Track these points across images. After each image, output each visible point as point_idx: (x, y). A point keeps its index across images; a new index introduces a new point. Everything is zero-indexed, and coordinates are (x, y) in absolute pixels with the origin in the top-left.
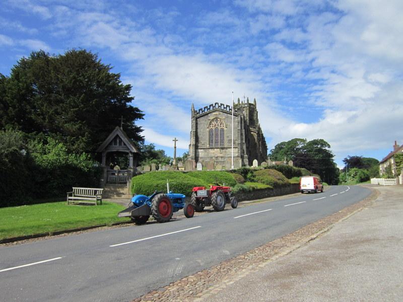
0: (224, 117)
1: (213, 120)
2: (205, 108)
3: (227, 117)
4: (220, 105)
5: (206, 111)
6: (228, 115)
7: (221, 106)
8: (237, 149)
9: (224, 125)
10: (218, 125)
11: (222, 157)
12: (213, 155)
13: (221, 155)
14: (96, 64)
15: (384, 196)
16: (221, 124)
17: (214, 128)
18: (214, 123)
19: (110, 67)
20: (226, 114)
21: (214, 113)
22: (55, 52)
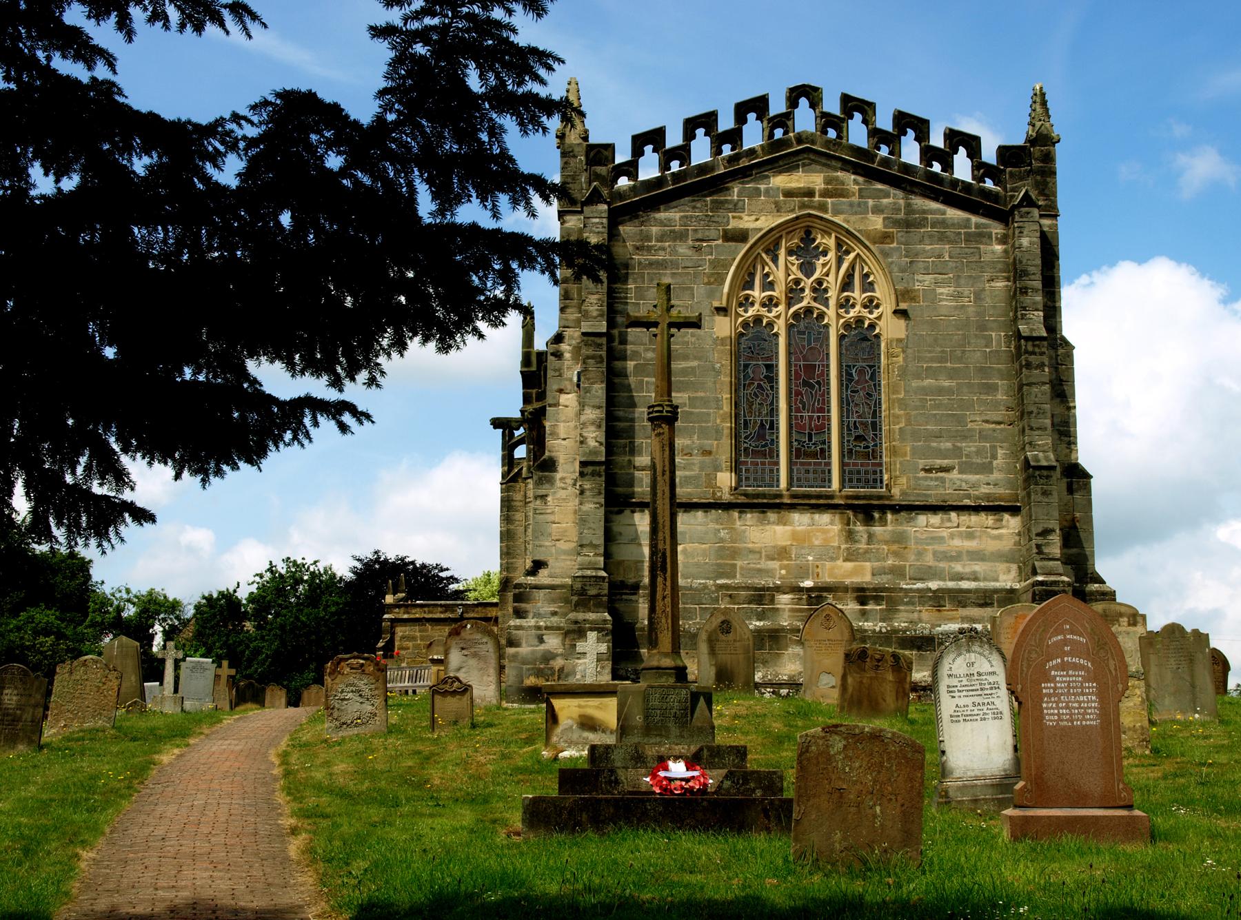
0: (877, 223)
1: (770, 243)
2: (742, 110)
3: (908, 225)
4: (937, 140)
5: (701, 151)
6: (919, 202)
7: (892, 140)
8: (1012, 523)
9: (883, 292)
10: (819, 290)
11: (863, 595)
12: (777, 573)
13: (862, 573)
14: (451, 206)
15: (542, 72)
16: (847, 285)
17: (780, 318)
18: (783, 269)
19: (105, 544)
20: (894, 198)
21: (780, 181)
22: (1077, 281)
